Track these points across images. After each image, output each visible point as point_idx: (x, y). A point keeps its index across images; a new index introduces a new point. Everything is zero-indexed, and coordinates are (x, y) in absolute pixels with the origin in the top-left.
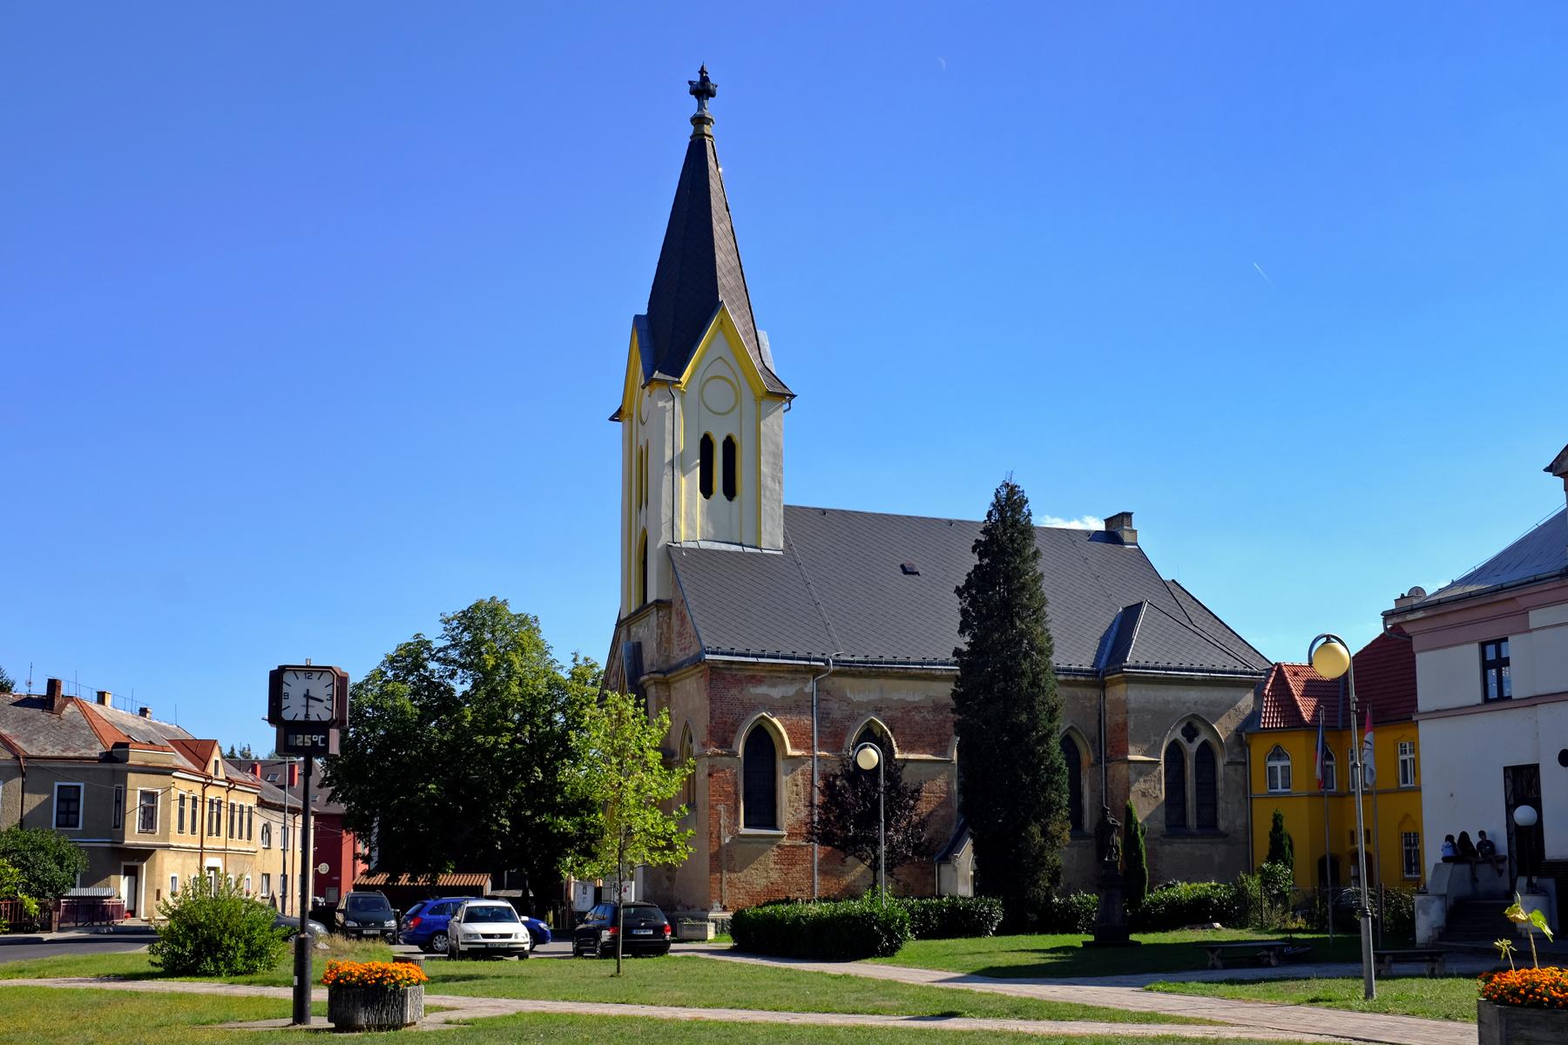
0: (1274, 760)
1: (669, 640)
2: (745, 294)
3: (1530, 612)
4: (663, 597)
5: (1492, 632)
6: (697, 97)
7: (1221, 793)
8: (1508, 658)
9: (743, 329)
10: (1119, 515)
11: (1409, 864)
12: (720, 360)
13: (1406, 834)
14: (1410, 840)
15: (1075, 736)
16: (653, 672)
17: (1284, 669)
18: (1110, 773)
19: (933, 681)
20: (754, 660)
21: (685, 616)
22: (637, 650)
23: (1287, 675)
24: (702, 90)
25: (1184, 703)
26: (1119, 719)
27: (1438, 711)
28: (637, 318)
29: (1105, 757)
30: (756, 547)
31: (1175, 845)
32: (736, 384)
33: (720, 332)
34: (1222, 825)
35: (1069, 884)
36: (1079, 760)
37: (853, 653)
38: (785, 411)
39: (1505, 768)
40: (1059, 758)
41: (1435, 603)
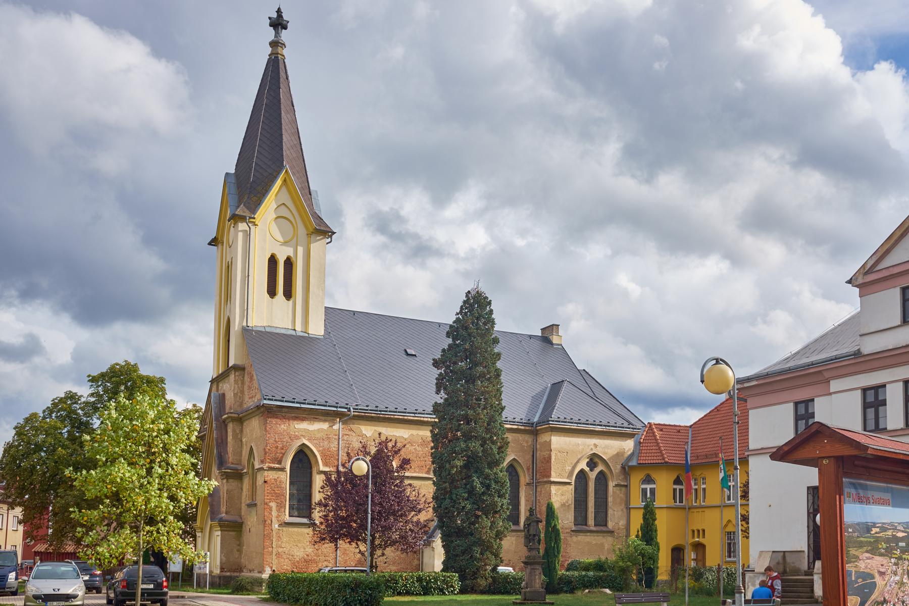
0: (644, 484)
1: (242, 392)
2: (303, 163)
3: (831, 382)
4: (239, 363)
5: (802, 394)
6: (274, 29)
7: (610, 504)
8: (814, 413)
9: (300, 186)
10: (551, 326)
11: (729, 552)
12: (283, 206)
13: (728, 533)
14: (731, 537)
15: (516, 465)
16: (231, 413)
17: (654, 427)
18: (539, 489)
19: (422, 425)
20: (298, 405)
21: (253, 376)
22: (222, 397)
23: (655, 430)
24: (278, 24)
25: (589, 446)
26: (546, 453)
27: (762, 449)
28: (227, 174)
29: (536, 480)
30: (305, 332)
31: (580, 537)
32: (294, 222)
33: (284, 186)
34: (610, 525)
35: (509, 560)
36: (519, 480)
37: (368, 403)
38: (327, 243)
39: (808, 488)
40: (504, 476)
41: (765, 374)
